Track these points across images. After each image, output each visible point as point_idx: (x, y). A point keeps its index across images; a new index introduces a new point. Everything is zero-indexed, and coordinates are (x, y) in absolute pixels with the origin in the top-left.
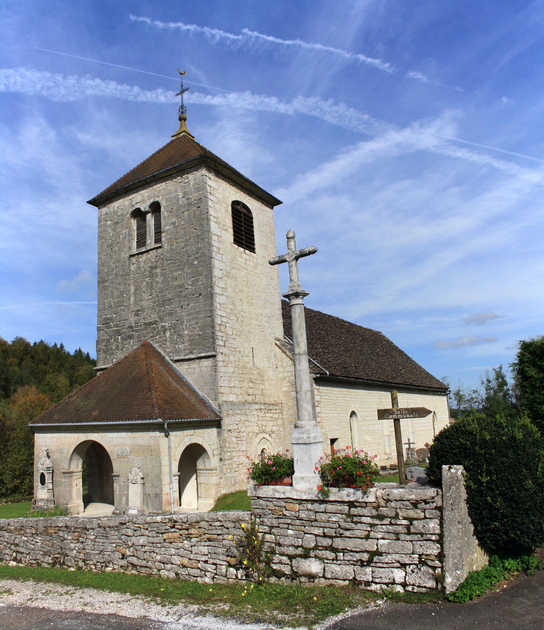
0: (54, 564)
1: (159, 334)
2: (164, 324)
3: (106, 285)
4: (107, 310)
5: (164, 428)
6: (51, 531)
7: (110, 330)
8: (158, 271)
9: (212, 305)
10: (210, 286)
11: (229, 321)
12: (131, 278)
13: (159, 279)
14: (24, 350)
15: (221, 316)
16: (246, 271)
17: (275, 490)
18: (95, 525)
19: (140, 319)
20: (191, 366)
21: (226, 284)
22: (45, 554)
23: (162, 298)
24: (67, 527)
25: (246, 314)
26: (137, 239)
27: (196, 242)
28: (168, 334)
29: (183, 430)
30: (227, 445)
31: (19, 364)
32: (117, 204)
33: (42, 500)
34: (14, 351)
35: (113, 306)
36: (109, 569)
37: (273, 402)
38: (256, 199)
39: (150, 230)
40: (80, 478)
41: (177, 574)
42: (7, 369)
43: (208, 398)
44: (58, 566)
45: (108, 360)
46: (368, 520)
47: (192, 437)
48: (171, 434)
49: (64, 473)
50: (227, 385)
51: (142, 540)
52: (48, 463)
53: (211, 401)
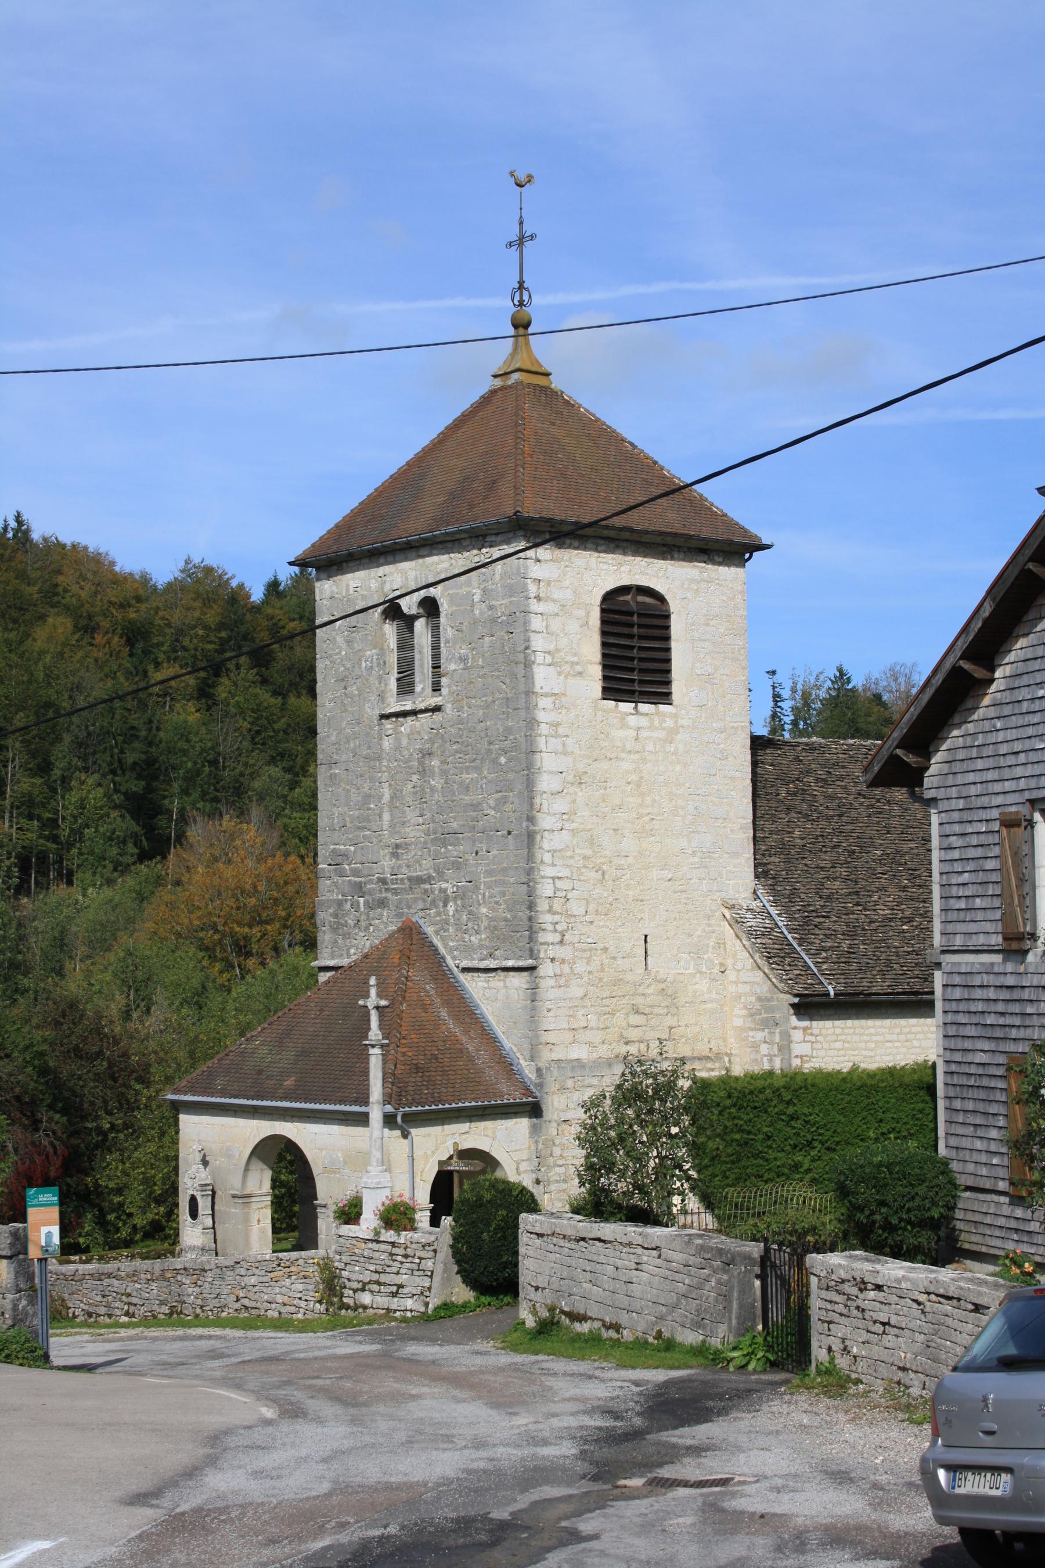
0: (171, 1314)
1: (436, 907)
2: (444, 885)
3: (336, 774)
4: (337, 834)
5: (396, 1122)
6: (168, 1275)
7: (343, 881)
8: (435, 763)
9: (530, 857)
10: (528, 816)
11: (577, 884)
12: (384, 769)
13: (437, 782)
14: (221, 626)
15: (553, 878)
16: (637, 756)
17: (350, 1230)
18: (213, 1266)
19: (400, 866)
20: (491, 984)
21: (574, 801)
22: (162, 1303)
23: (442, 827)
24: (185, 1269)
25: (630, 860)
26: (399, 673)
27: (504, 713)
28: (451, 908)
29: (443, 1124)
30: (557, 1151)
31: (204, 694)
32: (354, 579)
33: (193, 1248)
34: (180, 632)
35: (348, 824)
36: (224, 1314)
37: (706, 1053)
38: (684, 560)
39: (421, 660)
40: (266, 1207)
41: (280, 1313)
42: (150, 722)
43: (518, 1055)
44: (175, 1316)
45: (340, 948)
46: (399, 1258)
47: (464, 1136)
48: (414, 1131)
49: (234, 1196)
50: (565, 1026)
51: (253, 1280)
52: (203, 1175)
53: (522, 1061)
